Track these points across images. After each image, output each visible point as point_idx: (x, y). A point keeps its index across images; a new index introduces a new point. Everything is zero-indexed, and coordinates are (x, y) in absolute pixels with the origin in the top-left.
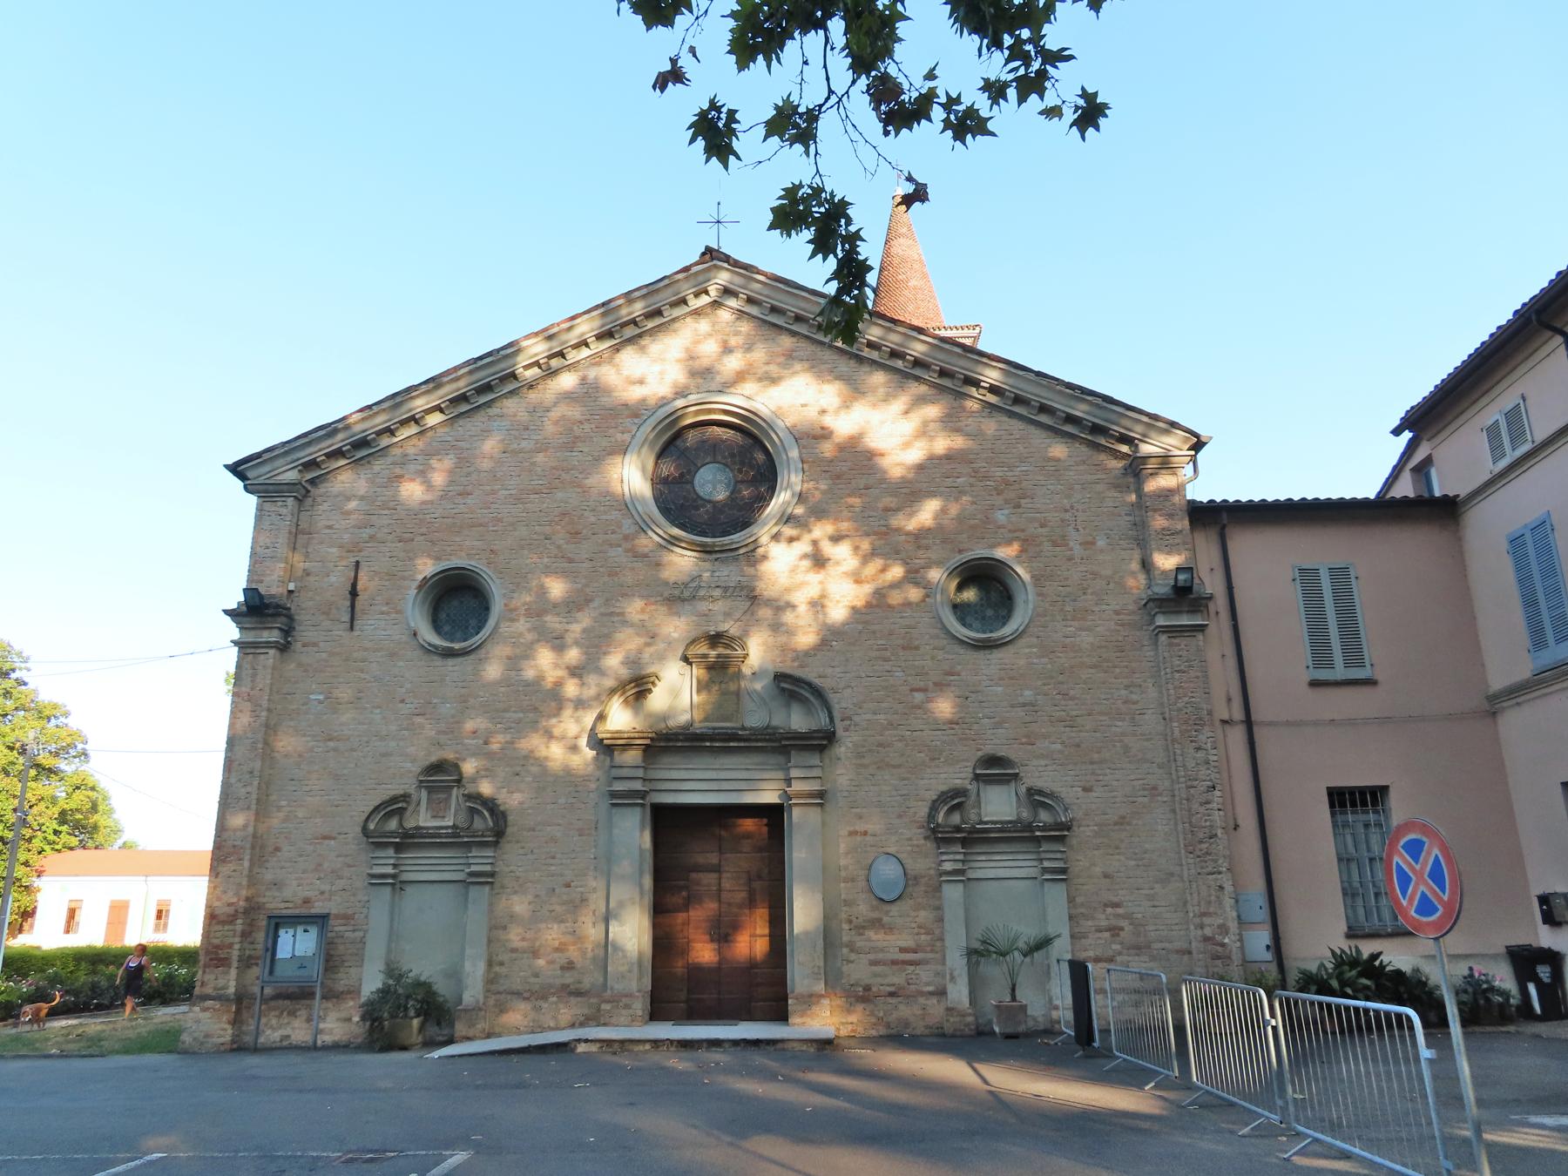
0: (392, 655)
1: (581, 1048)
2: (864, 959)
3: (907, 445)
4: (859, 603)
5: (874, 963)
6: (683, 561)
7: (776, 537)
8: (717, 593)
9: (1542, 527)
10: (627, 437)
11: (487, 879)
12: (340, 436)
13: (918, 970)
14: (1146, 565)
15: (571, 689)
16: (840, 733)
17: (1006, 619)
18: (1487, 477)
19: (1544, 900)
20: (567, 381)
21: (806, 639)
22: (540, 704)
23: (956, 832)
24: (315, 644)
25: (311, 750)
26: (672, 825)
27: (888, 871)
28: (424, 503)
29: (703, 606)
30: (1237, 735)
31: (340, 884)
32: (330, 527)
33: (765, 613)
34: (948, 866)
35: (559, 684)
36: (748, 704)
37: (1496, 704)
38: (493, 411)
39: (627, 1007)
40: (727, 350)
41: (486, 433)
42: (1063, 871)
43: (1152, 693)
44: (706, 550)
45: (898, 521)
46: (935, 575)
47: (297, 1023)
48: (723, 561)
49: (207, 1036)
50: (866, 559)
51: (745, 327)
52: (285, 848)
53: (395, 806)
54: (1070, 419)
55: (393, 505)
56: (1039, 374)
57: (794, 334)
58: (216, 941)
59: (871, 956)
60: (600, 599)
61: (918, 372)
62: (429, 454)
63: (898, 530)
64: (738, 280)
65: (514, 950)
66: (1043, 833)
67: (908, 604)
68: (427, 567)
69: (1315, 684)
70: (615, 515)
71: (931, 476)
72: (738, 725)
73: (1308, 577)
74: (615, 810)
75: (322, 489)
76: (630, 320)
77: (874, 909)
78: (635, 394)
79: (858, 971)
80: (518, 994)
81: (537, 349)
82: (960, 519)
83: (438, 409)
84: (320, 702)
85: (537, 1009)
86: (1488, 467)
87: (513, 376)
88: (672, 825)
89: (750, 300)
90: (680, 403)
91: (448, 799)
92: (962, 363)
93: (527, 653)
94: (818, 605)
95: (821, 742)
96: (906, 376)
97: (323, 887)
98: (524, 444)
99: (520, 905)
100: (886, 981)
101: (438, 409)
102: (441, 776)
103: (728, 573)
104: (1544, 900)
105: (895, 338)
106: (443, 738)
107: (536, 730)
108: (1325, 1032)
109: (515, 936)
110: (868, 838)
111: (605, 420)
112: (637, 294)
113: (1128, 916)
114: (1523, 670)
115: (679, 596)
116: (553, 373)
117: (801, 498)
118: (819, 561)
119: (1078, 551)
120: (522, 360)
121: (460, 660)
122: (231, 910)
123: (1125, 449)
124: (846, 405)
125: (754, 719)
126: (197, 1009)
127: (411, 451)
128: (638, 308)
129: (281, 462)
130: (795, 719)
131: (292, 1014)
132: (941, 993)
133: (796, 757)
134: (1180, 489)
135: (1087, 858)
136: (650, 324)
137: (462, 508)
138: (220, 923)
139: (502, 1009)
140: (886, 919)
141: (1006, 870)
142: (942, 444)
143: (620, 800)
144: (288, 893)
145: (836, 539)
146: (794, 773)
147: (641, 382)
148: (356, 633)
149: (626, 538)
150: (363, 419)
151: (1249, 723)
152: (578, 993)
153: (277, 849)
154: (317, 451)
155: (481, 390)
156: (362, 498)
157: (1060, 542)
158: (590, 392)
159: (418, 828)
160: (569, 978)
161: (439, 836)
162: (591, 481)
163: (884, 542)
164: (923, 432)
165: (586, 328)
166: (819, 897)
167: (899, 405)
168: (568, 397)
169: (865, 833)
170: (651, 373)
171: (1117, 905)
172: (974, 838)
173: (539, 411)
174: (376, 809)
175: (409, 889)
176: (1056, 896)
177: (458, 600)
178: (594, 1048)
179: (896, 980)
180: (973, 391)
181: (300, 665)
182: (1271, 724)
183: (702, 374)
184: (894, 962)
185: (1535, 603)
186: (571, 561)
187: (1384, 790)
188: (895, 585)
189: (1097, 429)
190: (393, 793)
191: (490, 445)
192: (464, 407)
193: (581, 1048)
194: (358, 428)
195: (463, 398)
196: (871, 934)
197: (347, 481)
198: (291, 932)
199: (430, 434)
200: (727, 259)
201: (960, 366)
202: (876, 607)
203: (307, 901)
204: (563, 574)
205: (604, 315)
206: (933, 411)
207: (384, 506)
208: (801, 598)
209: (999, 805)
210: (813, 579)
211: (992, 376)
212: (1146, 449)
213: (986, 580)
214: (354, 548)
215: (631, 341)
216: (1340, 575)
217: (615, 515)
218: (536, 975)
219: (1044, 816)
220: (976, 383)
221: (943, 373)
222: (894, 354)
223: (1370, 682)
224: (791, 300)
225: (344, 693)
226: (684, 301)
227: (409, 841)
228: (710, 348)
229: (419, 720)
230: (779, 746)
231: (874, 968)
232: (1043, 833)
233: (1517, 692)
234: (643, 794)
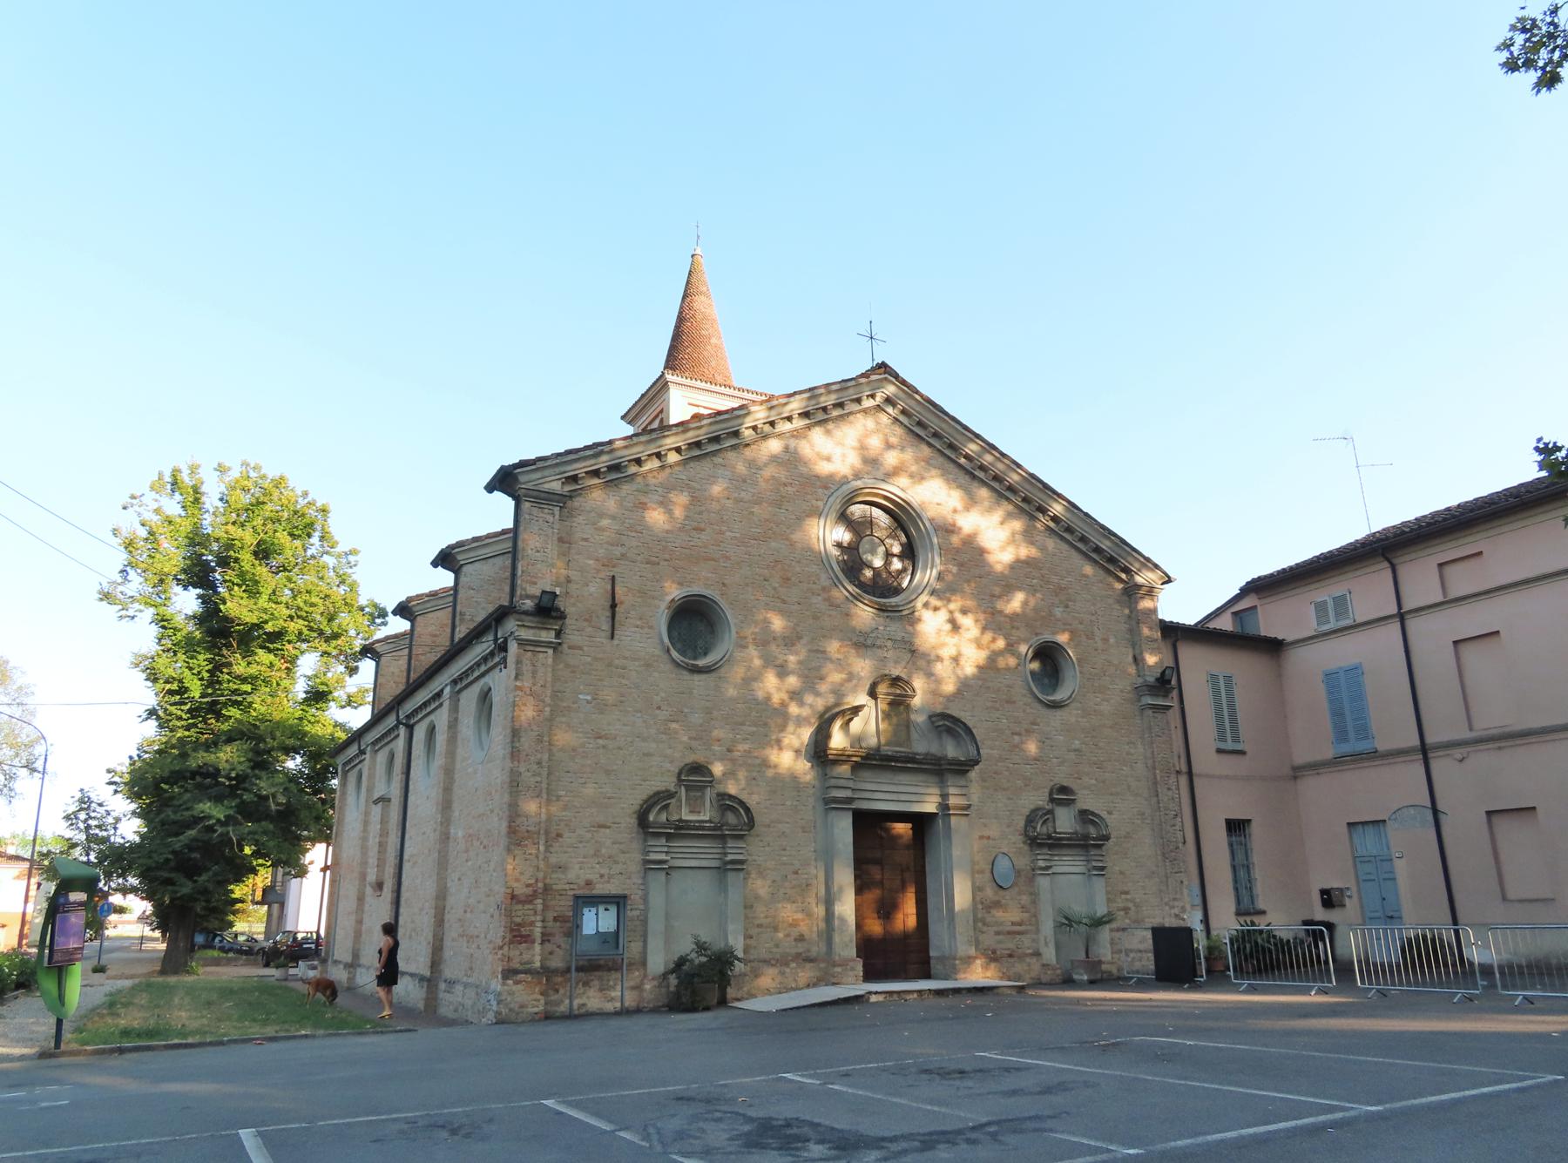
0: (648, 665)
1: (873, 998)
3: (1003, 549)
4: (981, 662)
5: (998, 933)
6: (864, 614)
7: (926, 605)
8: (889, 644)
9: (1355, 671)
10: (820, 504)
12: (604, 458)
13: (1023, 937)
14: (1137, 660)
15: (794, 709)
18: (1313, 633)
19: (1324, 892)
20: (774, 446)
21: (949, 687)
22: (767, 720)
23: (1041, 839)
24: (580, 648)
25: (583, 745)
26: (869, 824)
27: (1003, 865)
28: (667, 532)
29: (880, 652)
30: (1184, 780)
31: (617, 869)
32: (586, 540)
33: (922, 663)
34: (1041, 864)
35: (783, 704)
36: (914, 735)
37: (1297, 772)
38: (718, 460)
39: (853, 969)
40: (889, 446)
41: (713, 479)
42: (1103, 868)
43: (1140, 749)
44: (882, 609)
45: (1000, 605)
46: (1023, 648)
47: (591, 992)
48: (892, 618)
49: (522, 1007)
50: (984, 629)
51: (899, 430)
52: (566, 835)
53: (660, 799)
54: (1097, 550)
55: (640, 528)
56: (1086, 514)
57: (930, 445)
58: (518, 920)
60: (810, 633)
61: (1008, 494)
62: (669, 488)
63: (1001, 612)
64: (901, 394)
65: (760, 926)
66: (1089, 841)
67: (1008, 669)
68: (674, 592)
69: (1219, 751)
70: (814, 568)
71: (1021, 573)
73: (1214, 678)
75: (577, 502)
76: (826, 406)
78: (824, 468)
79: (989, 940)
80: (766, 962)
81: (759, 415)
82: (1035, 610)
83: (678, 450)
85: (782, 973)
86: (1311, 626)
87: (736, 434)
88: (869, 824)
89: (903, 412)
90: (859, 484)
91: (702, 797)
92: (1040, 495)
93: (756, 677)
94: (956, 660)
95: (961, 768)
96: (1000, 495)
98: (743, 494)
99: (761, 886)
101: (678, 450)
102: (695, 775)
103: (895, 628)
104: (1324, 892)
105: (1000, 466)
106: (694, 744)
108: (1446, 965)
109: (760, 910)
111: (806, 489)
112: (834, 387)
113: (1132, 901)
114: (1329, 753)
115: (863, 643)
116: (765, 437)
117: (940, 577)
118: (955, 627)
119: (1100, 644)
120: (749, 422)
121: (703, 676)
122: (529, 891)
123: (1123, 576)
124: (967, 509)
125: (920, 746)
126: (510, 982)
127: (652, 481)
128: (830, 400)
129: (551, 471)
130: (941, 745)
131: (586, 984)
132: (1037, 954)
134: (1155, 611)
135: (1113, 858)
136: (835, 413)
138: (519, 902)
139: (757, 974)
141: (1069, 865)
142: (1025, 551)
143: (831, 804)
144: (571, 875)
145: (964, 612)
146: (952, 790)
147: (828, 459)
148: (616, 642)
149: (824, 589)
150: (626, 447)
151: (1190, 774)
152: (811, 960)
153: (559, 835)
154: (580, 468)
155: (716, 439)
156: (614, 518)
157: (1090, 636)
158: (790, 459)
159: (680, 820)
160: (801, 948)
161: (703, 828)
162: (796, 536)
163: (994, 622)
164: (1012, 541)
165: (796, 405)
166: (969, 884)
167: (998, 515)
168: (774, 459)
170: (835, 451)
171: (1127, 893)
172: (1054, 844)
173: (752, 464)
175: (674, 874)
176: (1099, 885)
177: (694, 622)
178: (881, 998)
179: (1011, 946)
180: (1040, 516)
181: (567, 666)
182: (1207, 776)
183: (871, 462)
184: (1009, 933)
185: (1342, 715)
186: (784, 602)
187: (1249, 821)
188: (1000, 653)
189: (1112, 560)
190: (656, 789)
191: (716, 489)
192: (698, 453)
193: (873, 998)
194: (619, 454)
195: (698, 444)
196: (994, 912)
197: (598, 498)
198: (594, 910)
199: (668, 471)
200: (896, 376)
201: (1038, 497)
202: (989, 667)
203: (589, 883)
204: (781, 612)
205: (810, 398)
206: (1017, 525)
207: (631, 528)
208: (947, 652)
209: (1065, 821)
210: (953, 643)
211: (1057, 508)
212: (1139, 579)
213: (1048, 655)
214: (609, 563)
215: (821, 423)
216: (1228, 679)
217: (814, 568)
218: (777, 946)
219: (731, 818)
220: (1043, 510)
221: (1025, 500)
222: (996, 478)
223: (1242, 753)
224: (936, 421)
225: (609, 696)
226: (858, 401)
227: (681, 831)
228: (875, 442)
229: (674, 725)
230: (941, 770)
232: (1089, 841)
233: (1315, 767)
234: (850, 800)
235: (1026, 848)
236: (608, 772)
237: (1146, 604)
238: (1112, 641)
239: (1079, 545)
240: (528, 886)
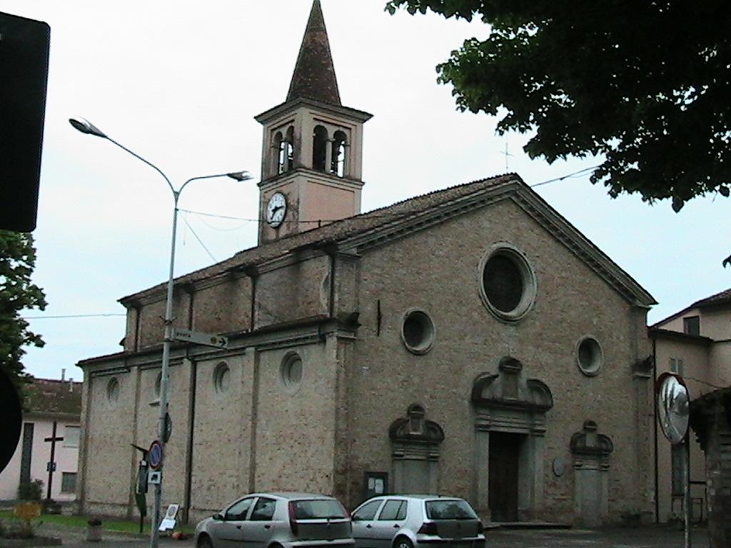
2: (551, 498)
11: (434, 459)
17: (512, 309)
56: (615, 264)
84: (367, 370)
97: (373, 460)
98: (441, 253)
106: (416, 394)
107: (586, 447)
137: (418, 281)
144: (360, 461)
203: (94, 412)
209: (590, 441)
216: (681, 361)
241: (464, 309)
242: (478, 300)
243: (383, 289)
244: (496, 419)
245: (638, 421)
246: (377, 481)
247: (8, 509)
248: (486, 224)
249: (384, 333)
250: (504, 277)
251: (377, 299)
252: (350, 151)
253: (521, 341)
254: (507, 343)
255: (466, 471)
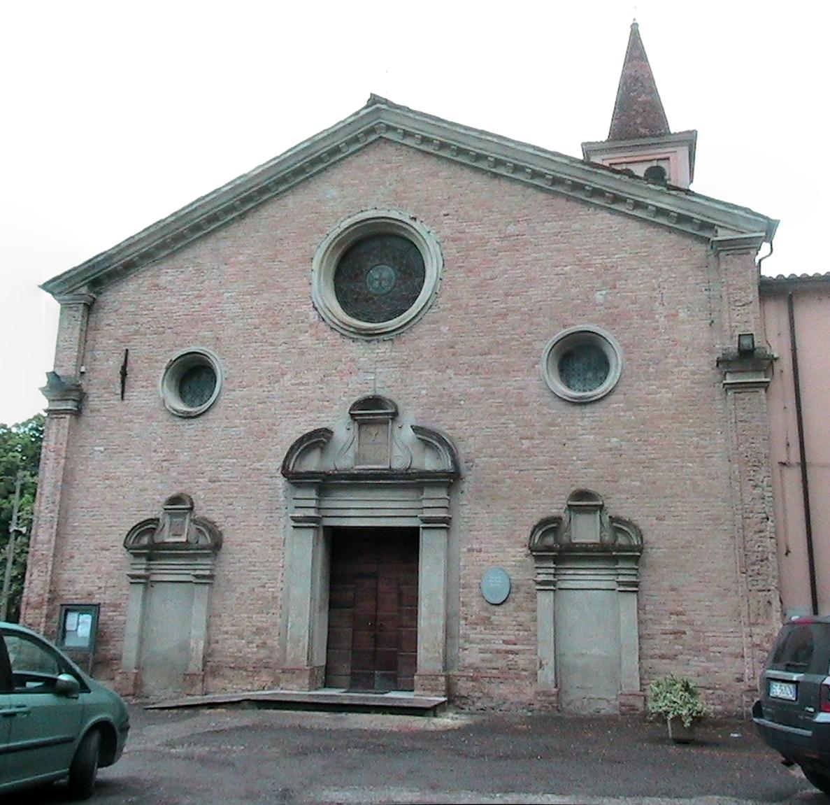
13: (517, 658)
16: (464, 472)
30: (794, 475)
52: (77, 556)
54: (660, 212)
59: (482, 646)
66: (621, 552)
72: (387, 467)
74: (296, 530)
77: (486, 610)
91: (183, 523)
98: (240, 258)
100: (494, 665)
110: (482, 554)
113: (691, 623)
133: (427, 493)
140: (493, 618)
141: (589, 588)
144: (78, 587)
148: (126, 402)
149: (311, 326)
153: (72, 557)
169: (480, 551)
174: (292, 448)
184: (498, 651)
203: (90, 594)
209: (586, 531)
231: (483, 655)
235: (530, 560)
236: (111, 506)
237: (541, 793)
238: (682, 315)
239: (536, 182)
240: (40, 595)
241: (282, 333)
242: (313, 314)
243: (136, 332)
244: (339, 505)
245: (675, 633)
246: (83, 617)
247: (186, 530)
248: (334, 192)
249: (134, 395)
250: (376, 270)
251: (124, 348)
252: (437, 273)
253: (405, 366)
254: (374, 368)
255: (274, 598)
